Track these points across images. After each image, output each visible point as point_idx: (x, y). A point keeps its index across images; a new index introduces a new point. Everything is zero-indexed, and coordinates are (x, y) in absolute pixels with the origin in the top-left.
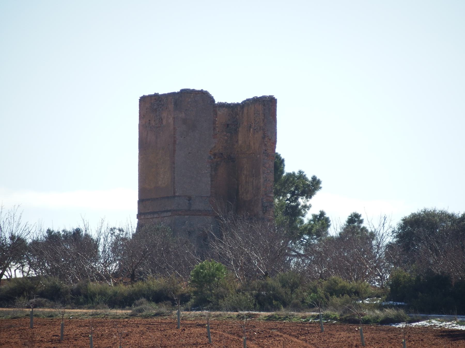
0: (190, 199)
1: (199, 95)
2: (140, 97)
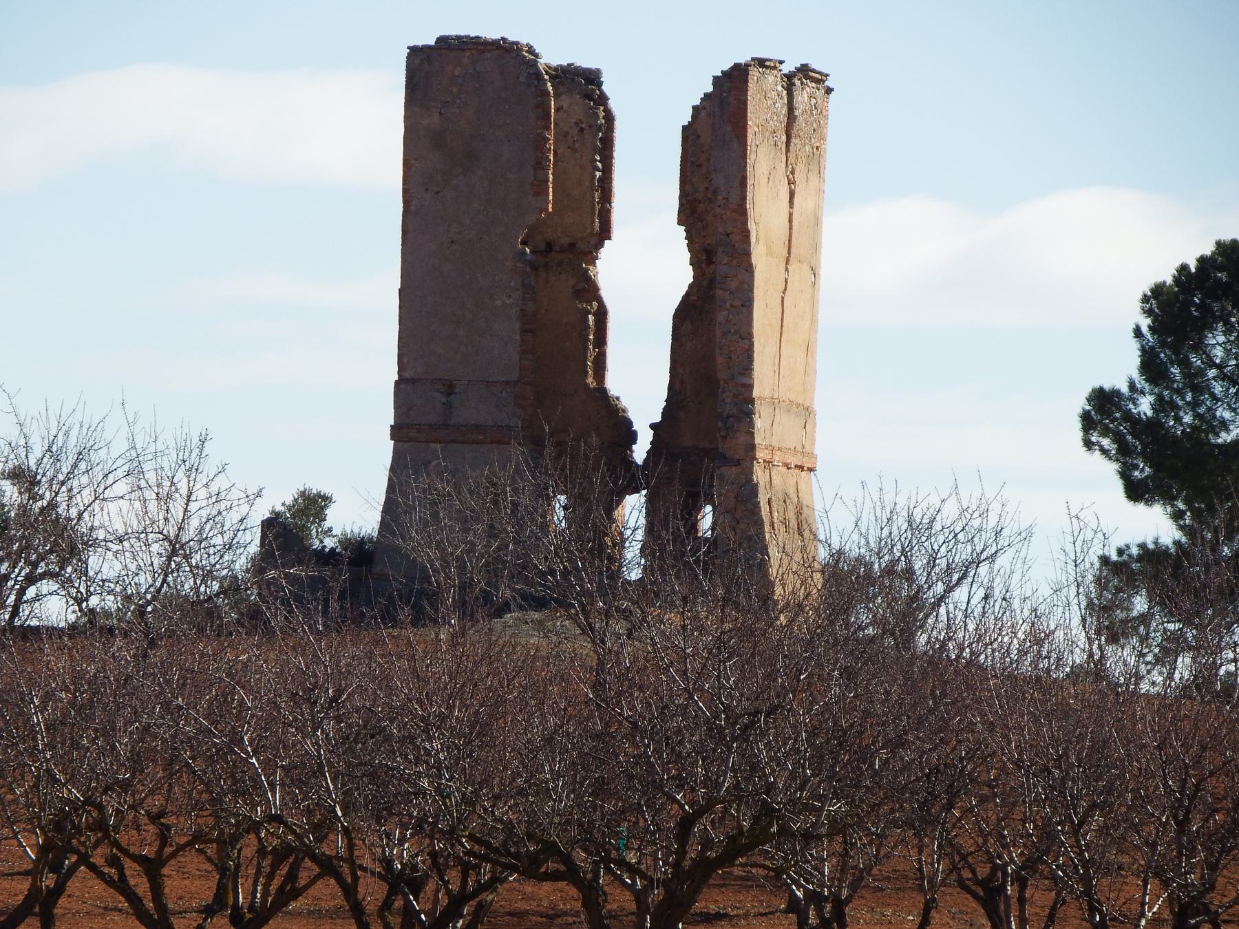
0: (449, 389)
1: (488, 55)
2: (408, 48)
